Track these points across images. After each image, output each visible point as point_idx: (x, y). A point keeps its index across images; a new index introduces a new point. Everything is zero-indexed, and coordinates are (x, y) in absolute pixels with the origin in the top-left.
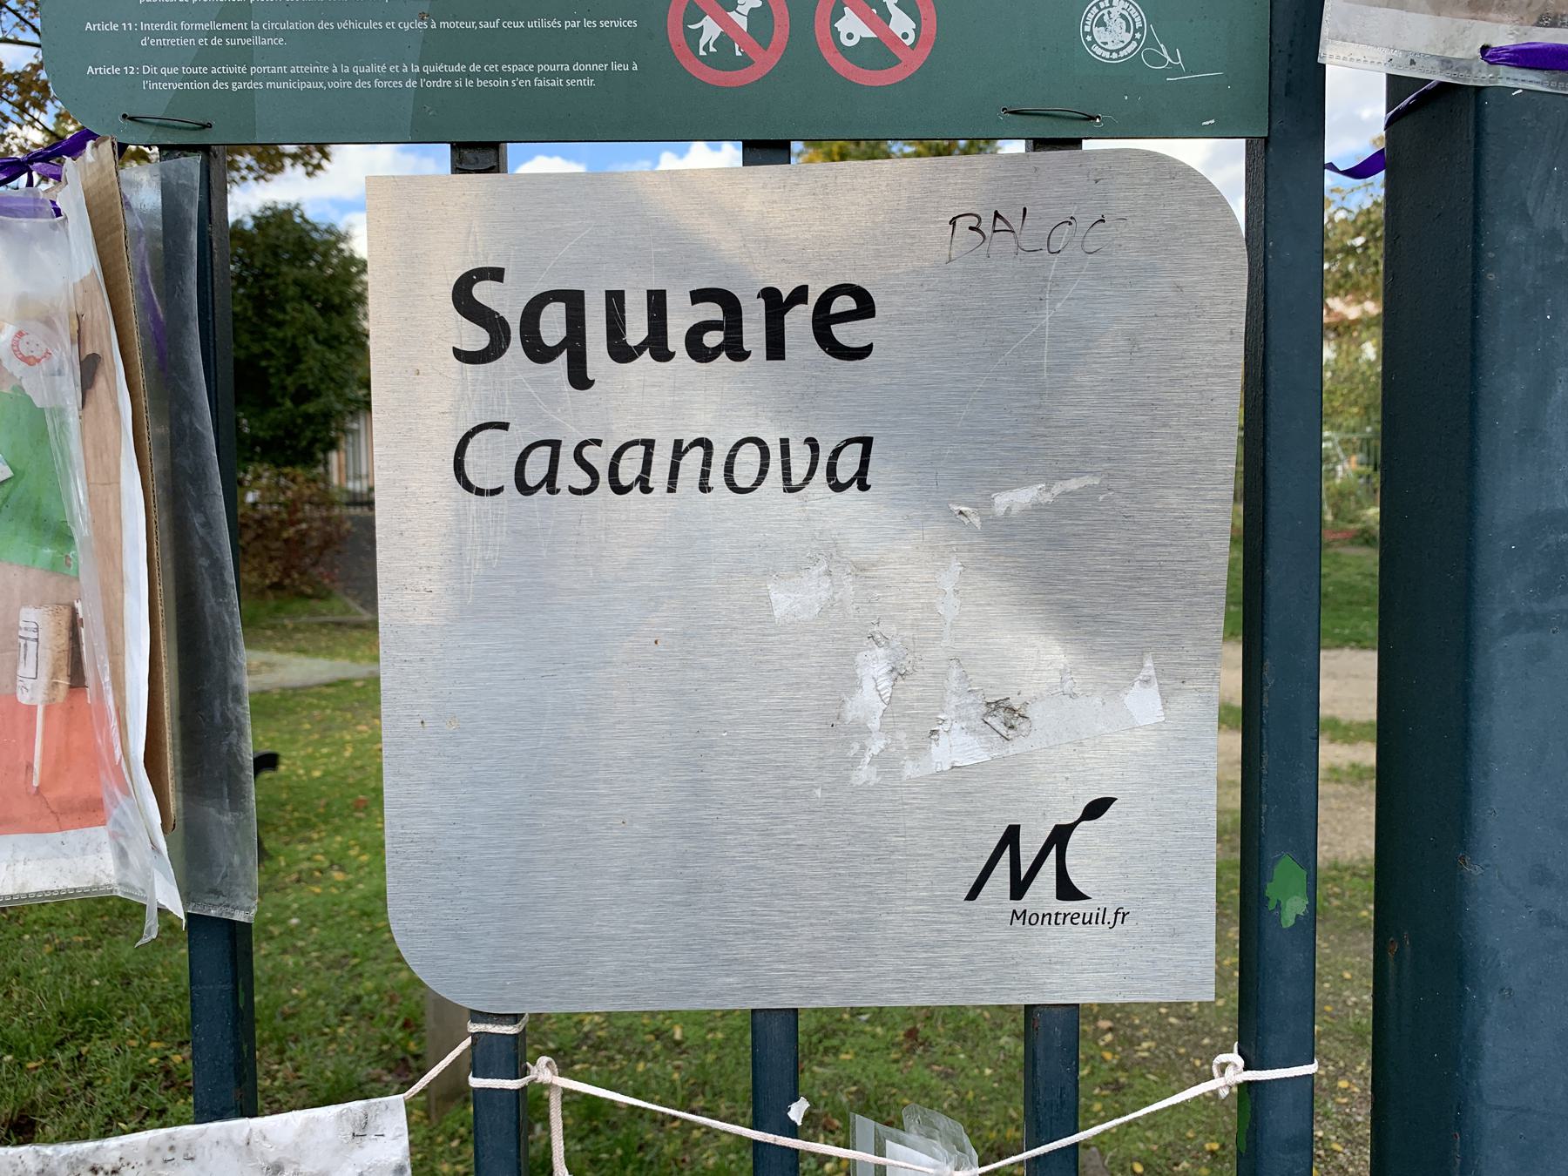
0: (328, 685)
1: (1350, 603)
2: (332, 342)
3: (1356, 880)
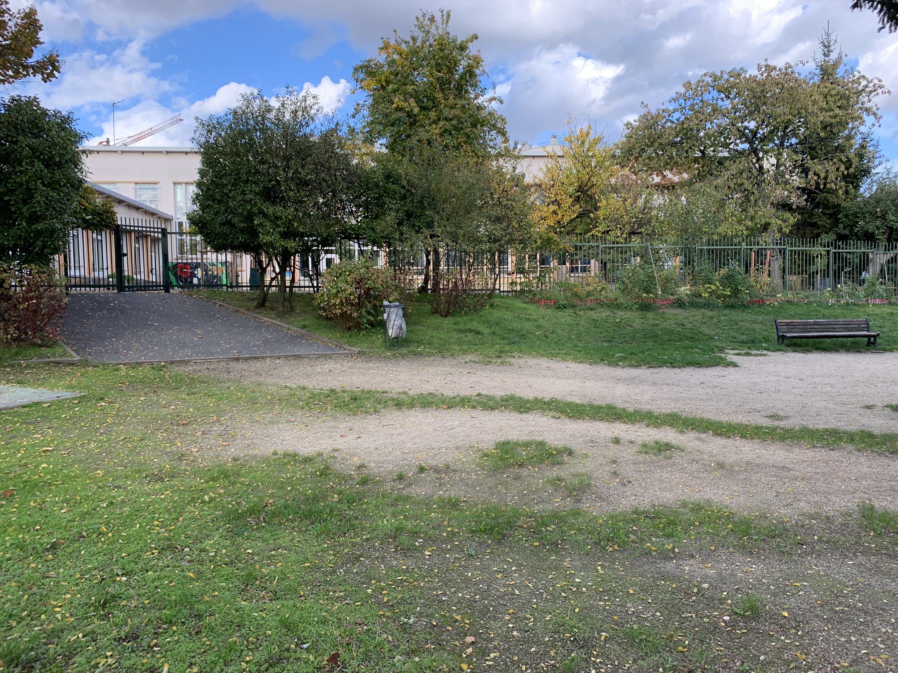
0: (24, 407)
1: (670, 340)
2: (52, 185)
3: (647, 520)
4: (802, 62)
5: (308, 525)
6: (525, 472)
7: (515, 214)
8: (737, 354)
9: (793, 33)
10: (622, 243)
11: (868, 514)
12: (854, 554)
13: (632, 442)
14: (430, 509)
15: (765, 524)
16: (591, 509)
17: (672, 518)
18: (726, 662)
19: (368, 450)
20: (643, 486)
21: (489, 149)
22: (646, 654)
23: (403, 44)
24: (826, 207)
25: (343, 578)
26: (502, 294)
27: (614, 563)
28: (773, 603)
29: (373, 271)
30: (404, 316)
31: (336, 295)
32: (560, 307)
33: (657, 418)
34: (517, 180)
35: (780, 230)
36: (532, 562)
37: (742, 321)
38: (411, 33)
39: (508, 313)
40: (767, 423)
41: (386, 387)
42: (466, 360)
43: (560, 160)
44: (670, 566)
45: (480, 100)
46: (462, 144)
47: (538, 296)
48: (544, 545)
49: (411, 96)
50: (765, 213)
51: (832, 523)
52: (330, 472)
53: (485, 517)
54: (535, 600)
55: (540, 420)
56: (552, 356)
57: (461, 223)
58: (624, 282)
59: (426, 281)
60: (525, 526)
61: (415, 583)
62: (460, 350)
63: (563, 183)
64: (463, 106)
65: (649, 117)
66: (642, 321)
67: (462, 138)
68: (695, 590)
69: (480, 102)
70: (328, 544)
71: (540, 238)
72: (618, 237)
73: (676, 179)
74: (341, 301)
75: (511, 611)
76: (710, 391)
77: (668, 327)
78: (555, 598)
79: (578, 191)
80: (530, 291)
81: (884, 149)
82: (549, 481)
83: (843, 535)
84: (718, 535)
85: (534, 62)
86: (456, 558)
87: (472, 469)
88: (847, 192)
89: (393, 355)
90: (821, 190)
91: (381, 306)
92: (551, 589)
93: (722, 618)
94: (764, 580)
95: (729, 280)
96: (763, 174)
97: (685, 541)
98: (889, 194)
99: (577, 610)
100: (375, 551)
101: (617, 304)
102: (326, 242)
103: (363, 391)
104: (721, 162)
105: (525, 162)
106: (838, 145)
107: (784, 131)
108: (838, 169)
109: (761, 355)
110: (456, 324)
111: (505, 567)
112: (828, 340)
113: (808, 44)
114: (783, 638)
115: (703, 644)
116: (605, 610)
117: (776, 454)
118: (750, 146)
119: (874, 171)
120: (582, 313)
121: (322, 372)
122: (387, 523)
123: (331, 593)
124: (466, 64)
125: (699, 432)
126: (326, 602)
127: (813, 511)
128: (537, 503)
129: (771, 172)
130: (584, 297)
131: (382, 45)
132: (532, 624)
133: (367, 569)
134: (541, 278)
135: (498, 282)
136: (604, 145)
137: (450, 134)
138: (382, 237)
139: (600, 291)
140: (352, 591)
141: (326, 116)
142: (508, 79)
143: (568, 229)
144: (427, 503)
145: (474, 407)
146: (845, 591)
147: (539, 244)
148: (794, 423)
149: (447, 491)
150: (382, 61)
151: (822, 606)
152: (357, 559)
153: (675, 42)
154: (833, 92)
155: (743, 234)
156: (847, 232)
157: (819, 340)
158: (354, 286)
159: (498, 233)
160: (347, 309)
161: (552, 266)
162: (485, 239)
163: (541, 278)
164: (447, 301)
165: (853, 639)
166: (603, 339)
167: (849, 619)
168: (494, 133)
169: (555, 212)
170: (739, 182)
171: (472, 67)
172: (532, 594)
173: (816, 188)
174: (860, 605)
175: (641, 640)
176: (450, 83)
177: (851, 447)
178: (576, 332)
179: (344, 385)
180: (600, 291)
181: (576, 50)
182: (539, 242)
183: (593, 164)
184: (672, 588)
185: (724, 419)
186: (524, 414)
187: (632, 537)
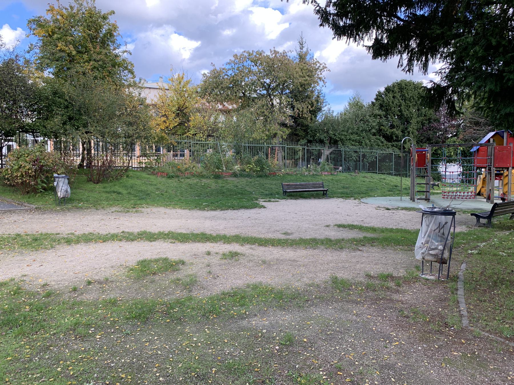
1: (231, 195)
3: (230, 297)
4: (290, 51)
5: (7, 330)
6: (157, 278)
7: (141, 121)
8: (265, 201)
9: (285, 36)
10: (203, 141)
11: (335, 280)
12: (332, 303)
13: (217, 253)
14: (97, 308)
15: (289, 292)
16: (198, 295)
17: (243, 295)
18: (280, 373)
19: (49, 274)
20: (225, 278)
21: (123, 81)
22: (239, 376)
23: (64, 10)
24: (302, 126)
25: (38, 363)
26: (134, 169)
27: (214, 326)
28: (298, 335)
29: (45, 154)
30: (69, 183)
31: (17, 170)
32: (170, 177)
33: (229, 238)
34: (142, 102)
35: (282, 137)
36: (167, 332)
37: (266, 184)
38: (69, 4)
39: (138, 181)
40: (283, 237)
41: (58, 230)
42: (112, 210)
43: (166, 91)
44: (245, 323)
45: (117, 51)
46: (106, 76)
47: (157, 171)
48: (173, 320)
49: (70, 43)
50: (275, 128)
51: (320, 288)
52: (21, 291)
53: (134, 308)
54: (171, 356)
55: (163, 245)
56: (166, 206)
57: (107, 125)
58: (205, 163)
59: (83, 161)
60: (160, 311)
61: (92, 358)
62: (108, 204)
63: (169, 105)
64: (106, 54)
65: (216, 72)
66: (216, 184)
67: (106, 73)
68: (260, 335)
69: (117, 52)
70: (24, 341)
71: (157, 137)
72: (201, 138)
73: (230, 107)
74: (22, 174)
75: (157, 365)
76: (253, 221)
77: (230, 188)
78: (183, 352)
79: (178, 110)
80: (151, 168)
81: (327, 98)
82: (172, 282)
83: (326, 293)
84: (267, 301)
85: (149, 33)
86: (118, 337)
87: (123, 279)
88: (311, 119)
89: (62, 209)
90: (300, 117)
91: (51, 177)
92: (180, 347)
93: (275, 348)
94: (293, 323)
95: (259, 162)
96: (273, 107)
97: (251, 307)
98: (330, 121)
99: (197, 358)
100: (60, 341)
101: (202, 175)
102: (8, 134)
103: (41, 234)
104: (254, 99)
105: (147, 91)
106: (308, 95)
107: (283, 86)
108: (307, 107)
109: (276, 201)
110: (104, 188)
111: (150, 338)
112: (306, 193)
113: (291, 42)
114: (305, 353)
115: (267, 365)
116: (212, 355)
117: (289, 253)
118: (267, 92)
119: (323, 109)
120: (182, 180)
121: (9, 223)
122: (68, 321)
123: (30, 376)
124: (107, 28)
125: (251, 244)
126: (27, 382)
127: (311, 282)
128: (166, 296)
129: (277, 107)
130: (184, 171)
131: (49, 8)
132: (171, 371)
133: (56, 354)
134: (158, 160)
135: (131, 162)
136: (192, 85)
137: (98, 70)
138: (52, 132)
139: (192, 168)
140: (46, 371)
141: (8, 50)
142: (133, 41)
143: (173, 132)
144: (95, 304)
145: (121, 240)
146: (331, 323)
147: (156, 139)
148: (295, 236)
149: (108, 295)
150: (49, 19)
151: (321, 333)
152: (48, 348)
153: (228, 33)
154: (305, 68)
155: (264, 138)
156: (312, 139)
157: (302, 193)
158: (31, 163)
159: (131, 132)
160: (26, 179)
161: (162, 153)
162: (123, 135)
163: (158, 160)
164: (97, 174)
165: (337, 348)
166: (195, 195)
167: (334, 338)
168: (126, 71)
169: (165, 122)
170: (262, 111)
171: (112, 30)
172: (169, 352)
173: (298, 116)
174: (338, 329)
175: (235, 369)
176: (97, 39)
177: (322, 247)
178: (179, 192)
179: (26, 231)
180: (192, 168)
181: (174, 29)
182: (156, 139)
183: (186, 96)
184: (248, 335)
185: (262, 236)
186: (153, 242)
187: (223, 309)
